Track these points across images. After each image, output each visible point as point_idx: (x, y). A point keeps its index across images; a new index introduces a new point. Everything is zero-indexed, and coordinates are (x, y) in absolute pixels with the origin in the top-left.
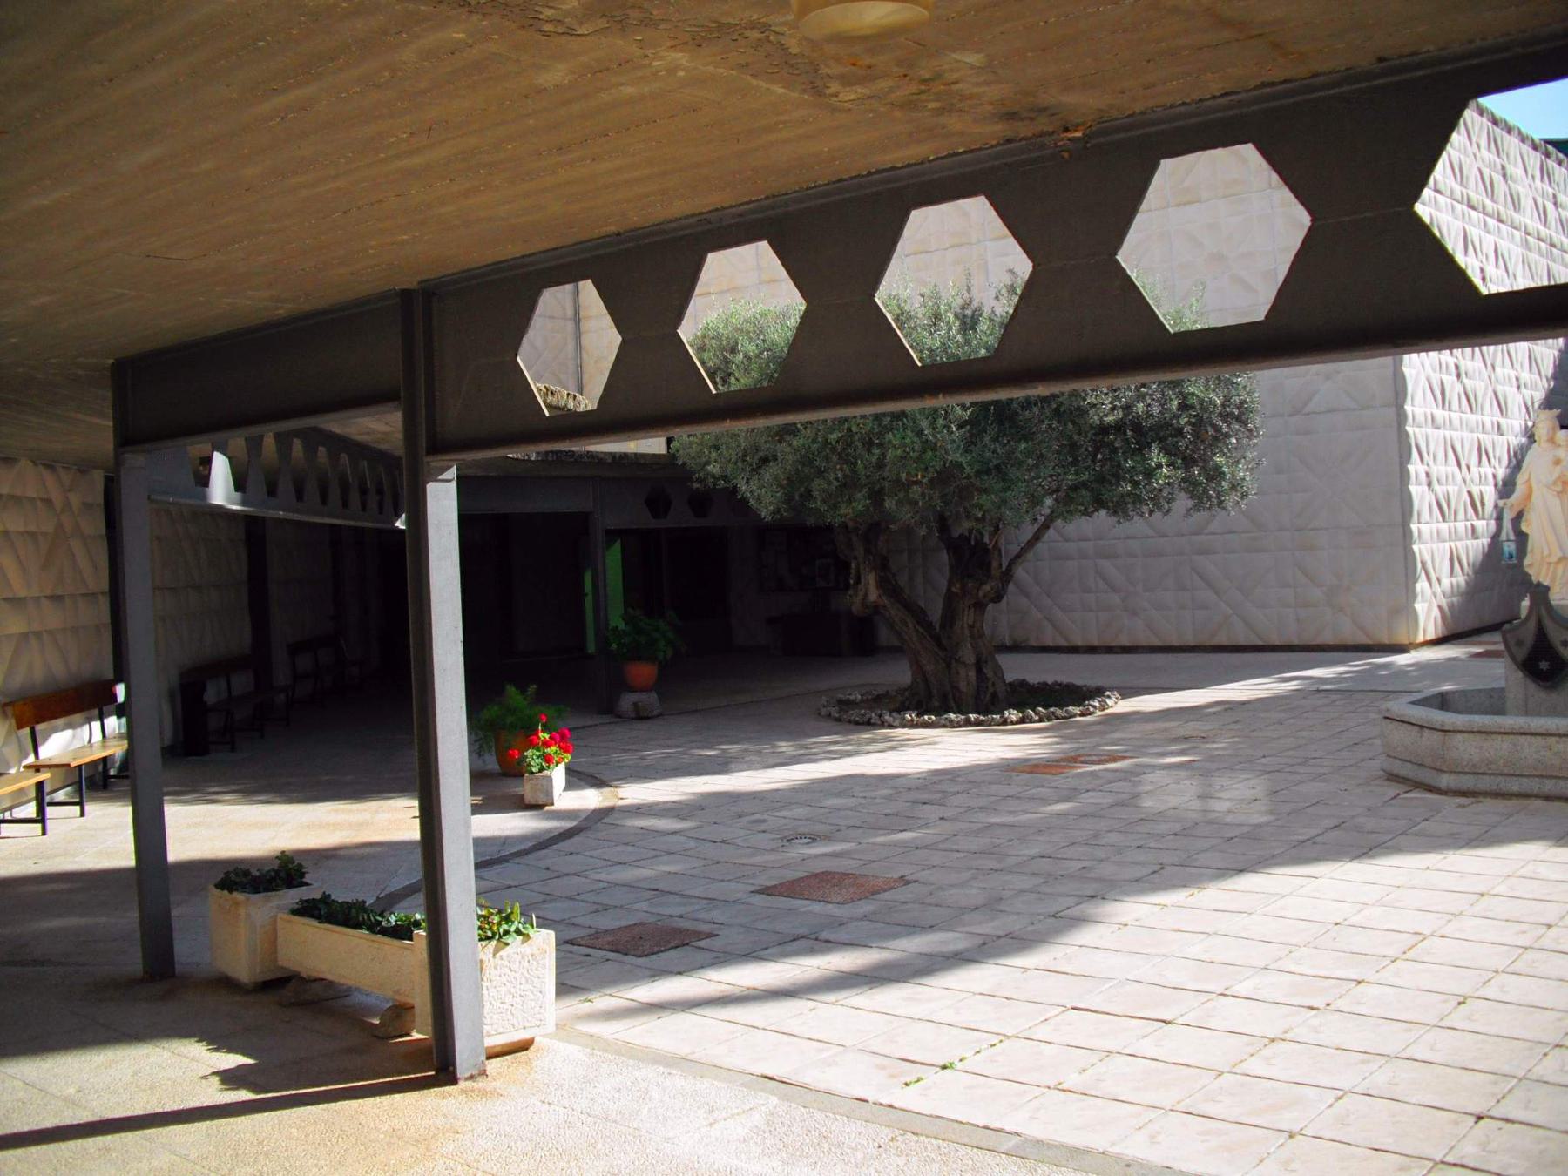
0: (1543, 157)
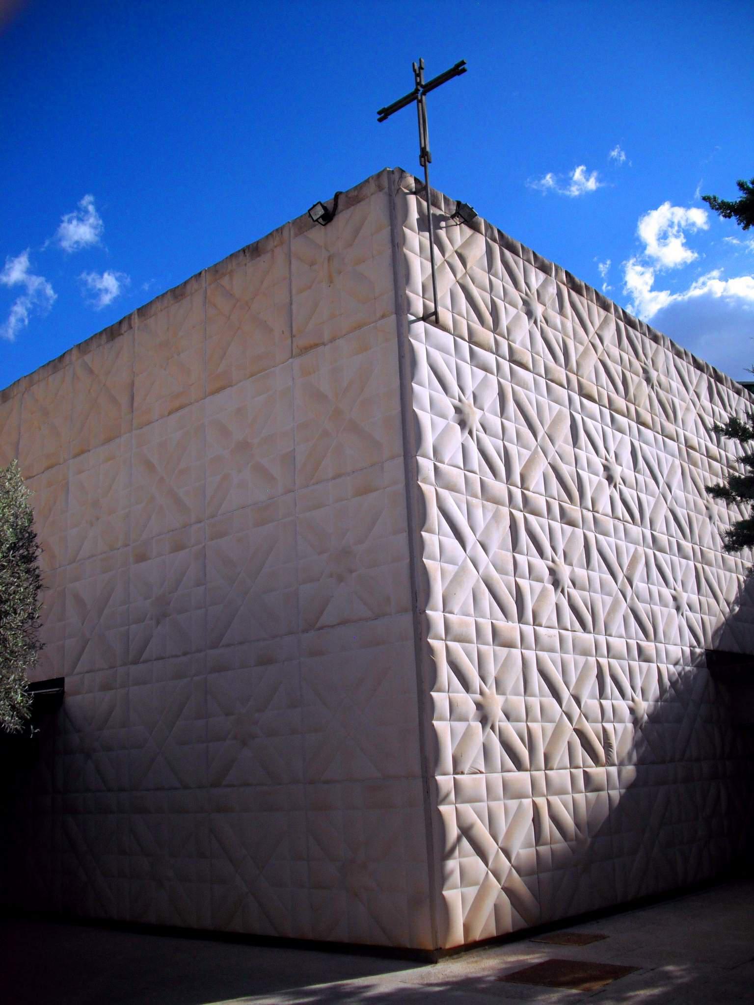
0: (712, 380)
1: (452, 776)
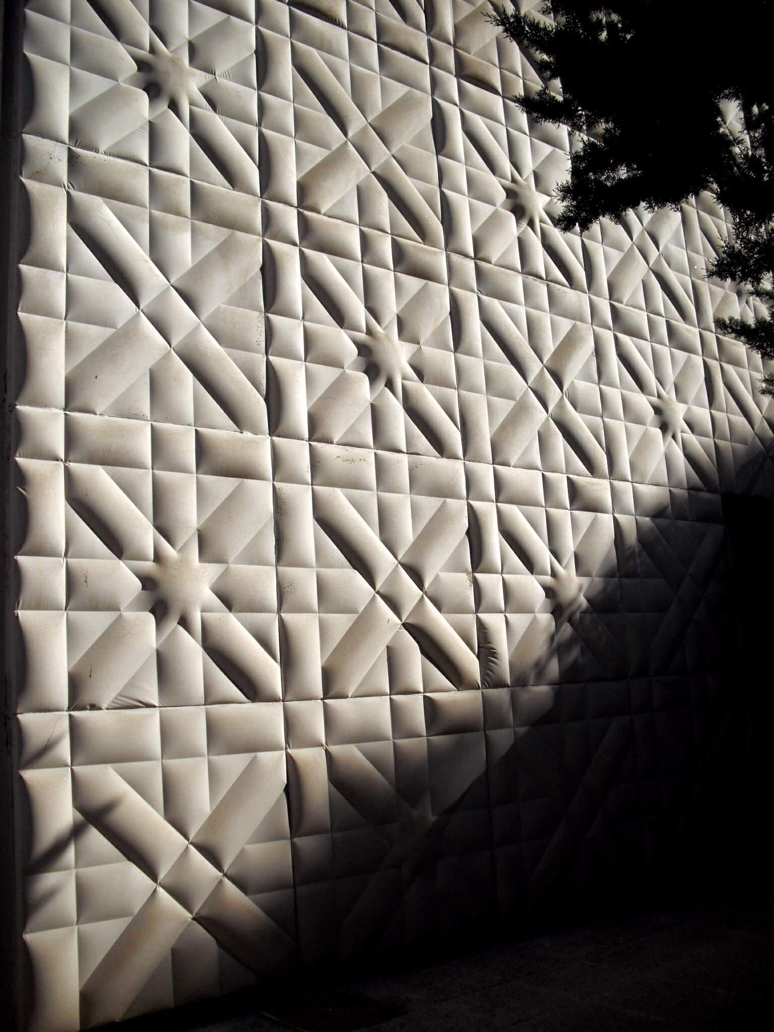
1: (66, 713)
